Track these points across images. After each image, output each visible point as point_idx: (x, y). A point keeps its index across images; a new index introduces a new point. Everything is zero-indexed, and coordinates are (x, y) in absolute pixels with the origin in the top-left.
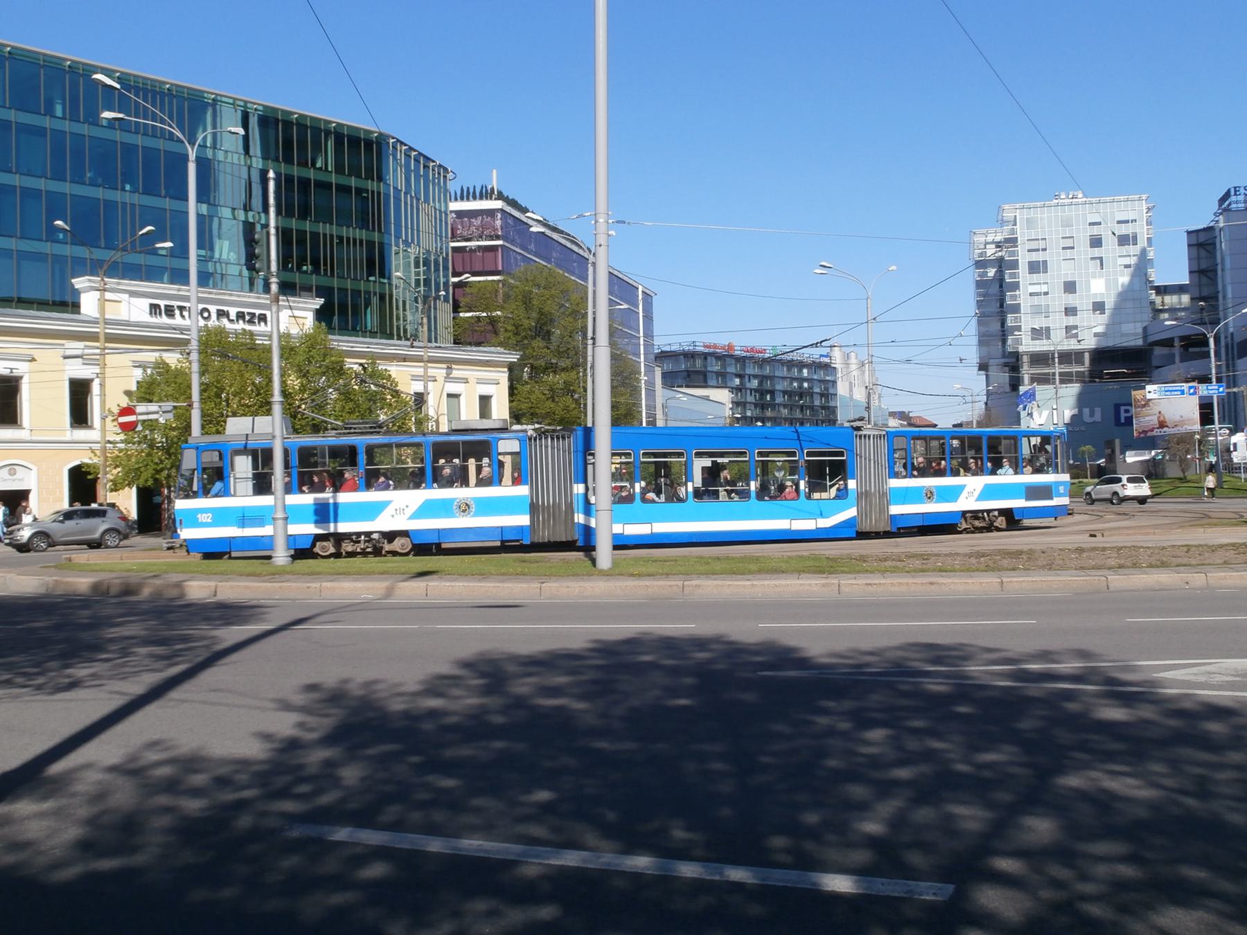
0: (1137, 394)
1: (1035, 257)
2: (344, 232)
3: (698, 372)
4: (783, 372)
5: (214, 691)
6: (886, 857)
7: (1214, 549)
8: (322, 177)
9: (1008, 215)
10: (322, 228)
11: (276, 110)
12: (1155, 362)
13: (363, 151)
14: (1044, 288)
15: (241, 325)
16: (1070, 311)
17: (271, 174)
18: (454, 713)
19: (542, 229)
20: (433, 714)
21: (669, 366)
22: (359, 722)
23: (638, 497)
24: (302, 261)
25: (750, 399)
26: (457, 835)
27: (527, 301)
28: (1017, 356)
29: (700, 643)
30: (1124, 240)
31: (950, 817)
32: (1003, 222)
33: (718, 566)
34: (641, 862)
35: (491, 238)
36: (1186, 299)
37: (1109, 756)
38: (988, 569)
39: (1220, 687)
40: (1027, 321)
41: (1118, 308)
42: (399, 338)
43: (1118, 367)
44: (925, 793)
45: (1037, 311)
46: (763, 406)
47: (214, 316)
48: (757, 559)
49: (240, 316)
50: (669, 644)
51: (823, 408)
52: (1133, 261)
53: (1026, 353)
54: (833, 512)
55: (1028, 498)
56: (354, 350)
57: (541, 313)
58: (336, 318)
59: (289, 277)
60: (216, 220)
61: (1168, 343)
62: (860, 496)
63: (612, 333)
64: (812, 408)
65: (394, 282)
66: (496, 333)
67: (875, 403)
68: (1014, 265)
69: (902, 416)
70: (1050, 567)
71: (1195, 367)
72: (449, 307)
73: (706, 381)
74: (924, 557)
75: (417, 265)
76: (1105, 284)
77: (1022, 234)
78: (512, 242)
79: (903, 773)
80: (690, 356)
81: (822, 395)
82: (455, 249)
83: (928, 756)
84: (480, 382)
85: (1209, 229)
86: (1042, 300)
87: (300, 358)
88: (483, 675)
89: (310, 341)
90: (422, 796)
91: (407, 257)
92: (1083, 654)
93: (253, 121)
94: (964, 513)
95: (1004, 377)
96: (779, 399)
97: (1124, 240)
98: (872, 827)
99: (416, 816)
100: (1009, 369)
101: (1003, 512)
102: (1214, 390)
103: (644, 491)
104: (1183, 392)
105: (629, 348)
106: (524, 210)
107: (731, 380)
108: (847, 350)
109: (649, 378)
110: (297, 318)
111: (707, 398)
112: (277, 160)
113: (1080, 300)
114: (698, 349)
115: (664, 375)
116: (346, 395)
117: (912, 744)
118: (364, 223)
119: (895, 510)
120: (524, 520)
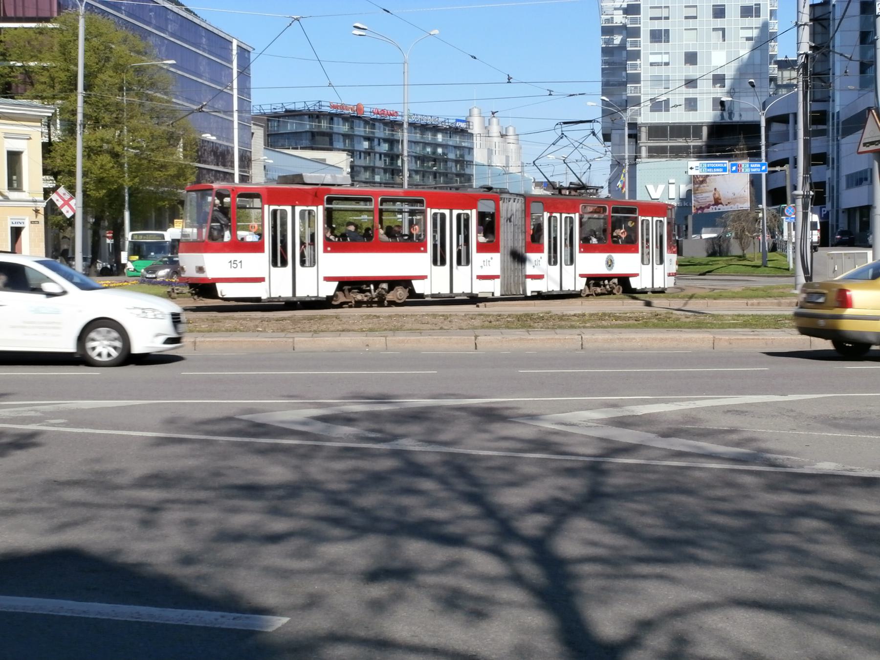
3: (323, 134)
5: (742, 412)
14: (665, 59)
25: (379, 163)
30: (747, 12)
40: (646, 91)
45: (656, 80)
51: (458, 175)
52: (755, 33)
53: (645, 125)
73: (331, 143)
76: (724, 56)
80: (316, 116)
81: (457, 162)
84: (8, 136)
86: (662, 71)
97: (747, 12)
104: (725, 169)
107: (360, 143)
111: (322, 162)
114: (324, 109)
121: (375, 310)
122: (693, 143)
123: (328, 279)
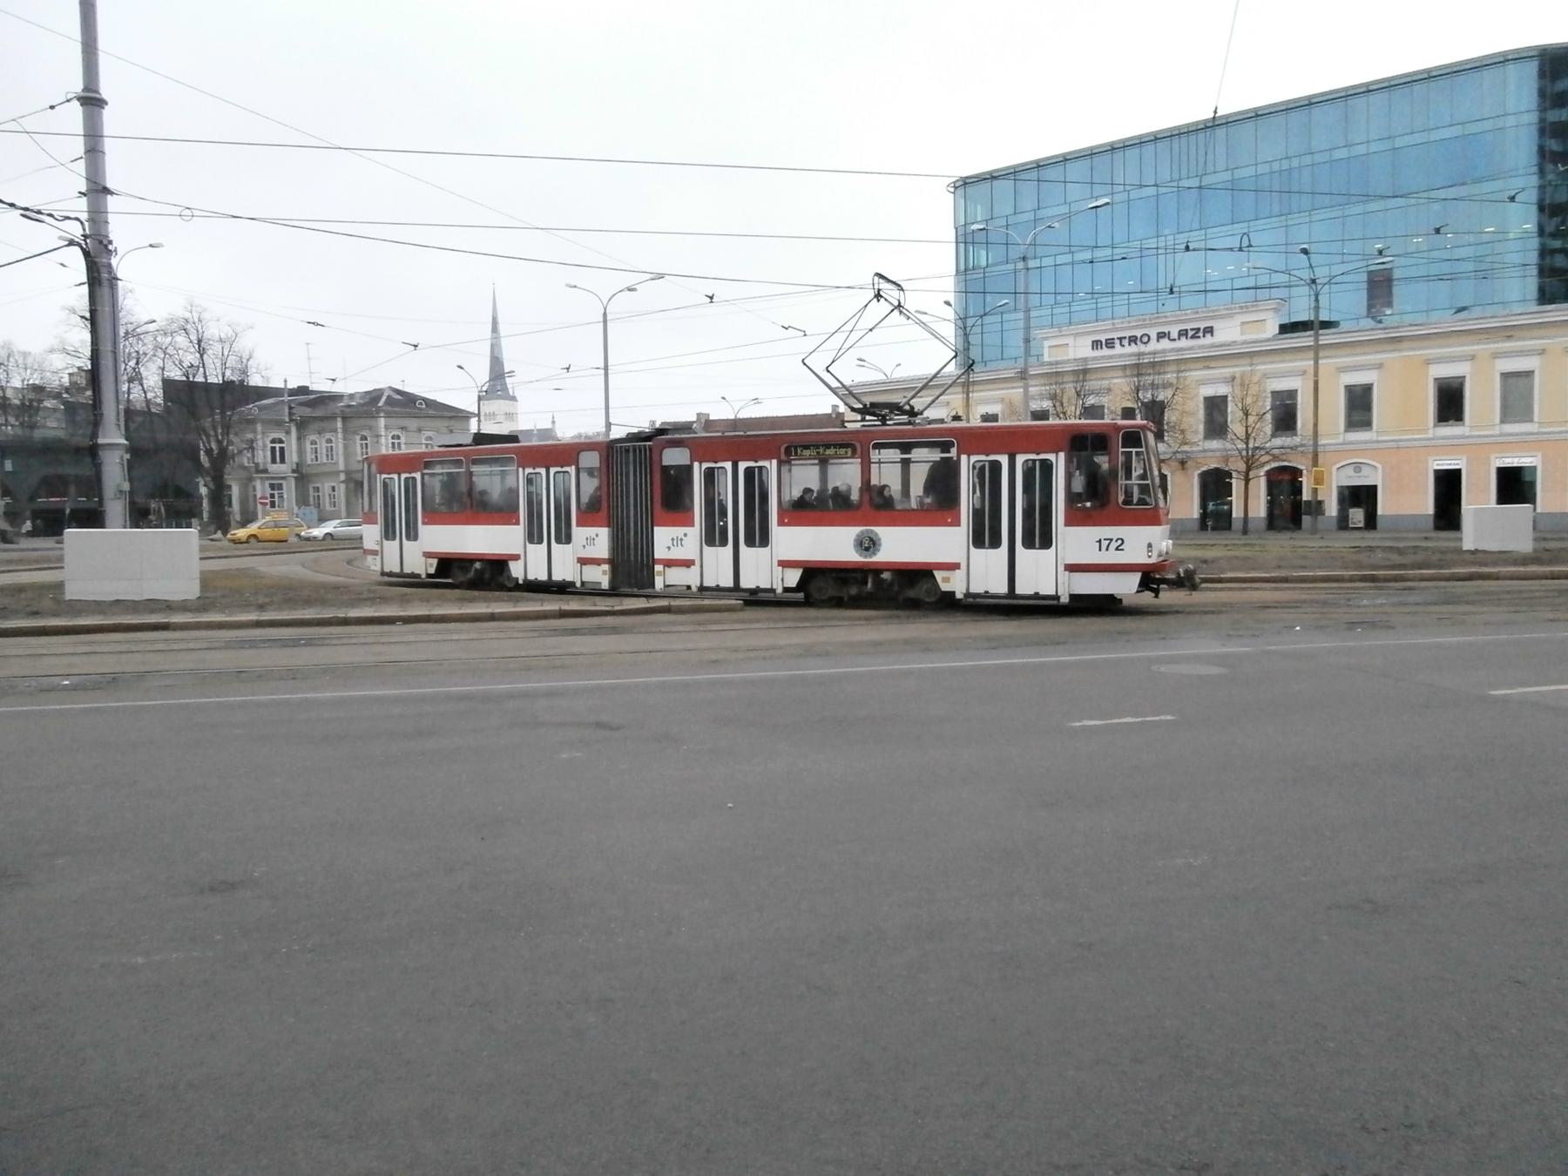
47: (1154, 337)
49: (1183, 333)
123: (785, 564)
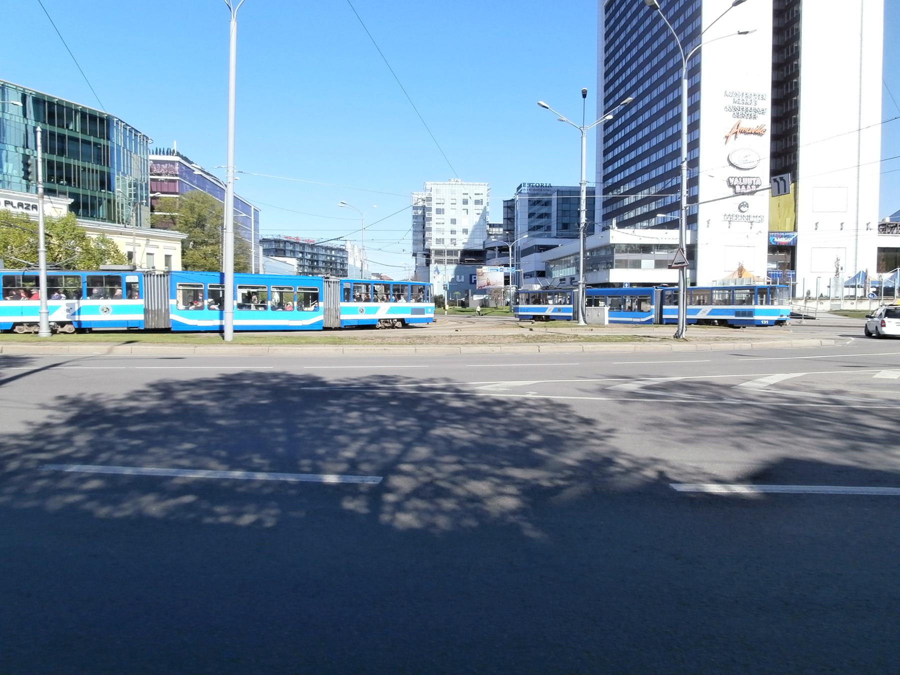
0: (479, 270)
1: (439, 207)
2: (86, 165)
4: (323, 252)
6: (353, 466)
7: (505, 337)
8: (73, 134)
9: (428, 187)
10: (72, 162)
11: (44, 95)
12: (487, 257)
13: (98, 123)
14: (442, 221)
15: (20, 210)
16: (453, 232)
17: (39, 129)
18: (143, 409)
19: (201, 173)
20: (131, 409)
21: (266, 246)
22: (88, 414)
23: (206, 307)
24: (60, 178)
25: (307, 264)
26: (140, 466)
27: (192, 209)
28: (429, 250)
29: (275, 375)
30: (477, 202)
31: (384, 449)
32: (426, 190)
33: (286, 340)
34: (238, 474)
35: (173, 175)
36: (501, 230)
37: (454, 422)
38: (410, 343)
39: (501, 393)
41: (473, 232)
42: (119, 222)
43: (473, 257)
44: (373, 439)
45: (439, 230)
46: (313, 268)
48: (305, 338)
49: (20, 205)
50: (259, 376)
52: (481, 212)
54: (311, 317)
55: (412, 314)
56: (93, 229)
57: (199, 215)
58: (81, 210)
59: (51, 186)
60: (4, 152)
61: (492, 249)
62: (325, 310)
63: (236, 227)
64: (336, 269)
65: (117, 194)
66: (175, 224)
67: (365, 268)
68: (430, 209)
69: (378, 275)
70: (437, 343)
71: (503, 260)
72: (149, 209)
74: (383, 338)
75: (130, 186)
76: (469, 220)
77: (434, 196)
78: (185, 178)
79: (364, 431)
80: (277, 241)
82: (152, 180)
83: (377, 423)
85: (513, 200)
87: (59, 230)
88: (160, 390)
89: (65, 223)
90: (122, 448)
91: (124, 181)
92: (447, 380)
93: (29, 101)
94: (379, 320)
95: (424, 259)
96: (321, 265)
97: (477, 202)
98: (349, 454)
99: (118, 457)
100: (426, 256)
101: (399, 320)
102: (510, 270)
103: (210, 304)
105: (246, 236)
106: (191, 163)
108: (353, 243)
109: (256, 253)
110: (57, 208)
111: (285, 262)
112: (45, 122)
113: (458, 227)
115: (264, 250)
116: (87, 251)
117: (370, 418)
118: (98, 160)
119: (343, 317)
120: (141, 317)
121: (391, 330)
122: (454, 258)
